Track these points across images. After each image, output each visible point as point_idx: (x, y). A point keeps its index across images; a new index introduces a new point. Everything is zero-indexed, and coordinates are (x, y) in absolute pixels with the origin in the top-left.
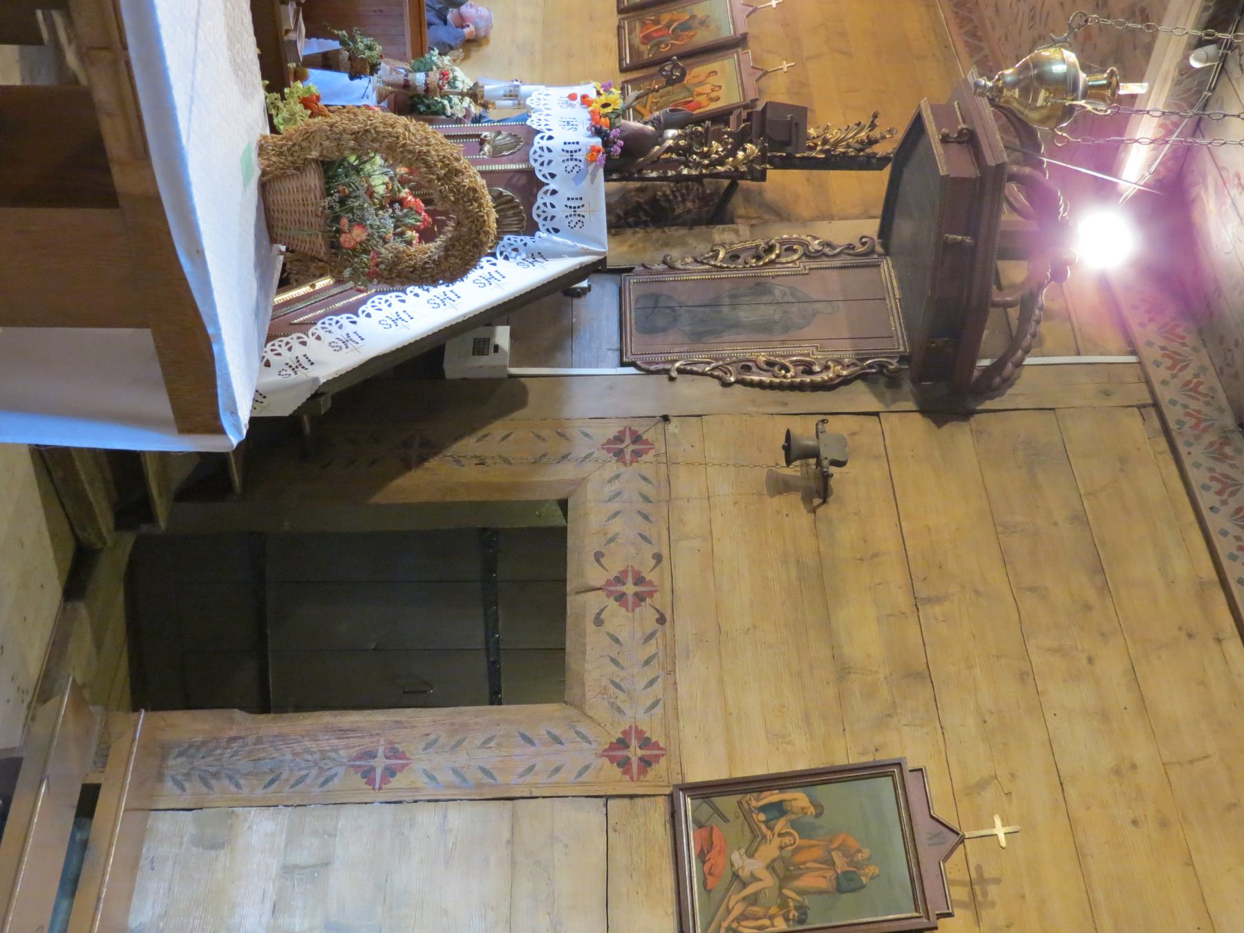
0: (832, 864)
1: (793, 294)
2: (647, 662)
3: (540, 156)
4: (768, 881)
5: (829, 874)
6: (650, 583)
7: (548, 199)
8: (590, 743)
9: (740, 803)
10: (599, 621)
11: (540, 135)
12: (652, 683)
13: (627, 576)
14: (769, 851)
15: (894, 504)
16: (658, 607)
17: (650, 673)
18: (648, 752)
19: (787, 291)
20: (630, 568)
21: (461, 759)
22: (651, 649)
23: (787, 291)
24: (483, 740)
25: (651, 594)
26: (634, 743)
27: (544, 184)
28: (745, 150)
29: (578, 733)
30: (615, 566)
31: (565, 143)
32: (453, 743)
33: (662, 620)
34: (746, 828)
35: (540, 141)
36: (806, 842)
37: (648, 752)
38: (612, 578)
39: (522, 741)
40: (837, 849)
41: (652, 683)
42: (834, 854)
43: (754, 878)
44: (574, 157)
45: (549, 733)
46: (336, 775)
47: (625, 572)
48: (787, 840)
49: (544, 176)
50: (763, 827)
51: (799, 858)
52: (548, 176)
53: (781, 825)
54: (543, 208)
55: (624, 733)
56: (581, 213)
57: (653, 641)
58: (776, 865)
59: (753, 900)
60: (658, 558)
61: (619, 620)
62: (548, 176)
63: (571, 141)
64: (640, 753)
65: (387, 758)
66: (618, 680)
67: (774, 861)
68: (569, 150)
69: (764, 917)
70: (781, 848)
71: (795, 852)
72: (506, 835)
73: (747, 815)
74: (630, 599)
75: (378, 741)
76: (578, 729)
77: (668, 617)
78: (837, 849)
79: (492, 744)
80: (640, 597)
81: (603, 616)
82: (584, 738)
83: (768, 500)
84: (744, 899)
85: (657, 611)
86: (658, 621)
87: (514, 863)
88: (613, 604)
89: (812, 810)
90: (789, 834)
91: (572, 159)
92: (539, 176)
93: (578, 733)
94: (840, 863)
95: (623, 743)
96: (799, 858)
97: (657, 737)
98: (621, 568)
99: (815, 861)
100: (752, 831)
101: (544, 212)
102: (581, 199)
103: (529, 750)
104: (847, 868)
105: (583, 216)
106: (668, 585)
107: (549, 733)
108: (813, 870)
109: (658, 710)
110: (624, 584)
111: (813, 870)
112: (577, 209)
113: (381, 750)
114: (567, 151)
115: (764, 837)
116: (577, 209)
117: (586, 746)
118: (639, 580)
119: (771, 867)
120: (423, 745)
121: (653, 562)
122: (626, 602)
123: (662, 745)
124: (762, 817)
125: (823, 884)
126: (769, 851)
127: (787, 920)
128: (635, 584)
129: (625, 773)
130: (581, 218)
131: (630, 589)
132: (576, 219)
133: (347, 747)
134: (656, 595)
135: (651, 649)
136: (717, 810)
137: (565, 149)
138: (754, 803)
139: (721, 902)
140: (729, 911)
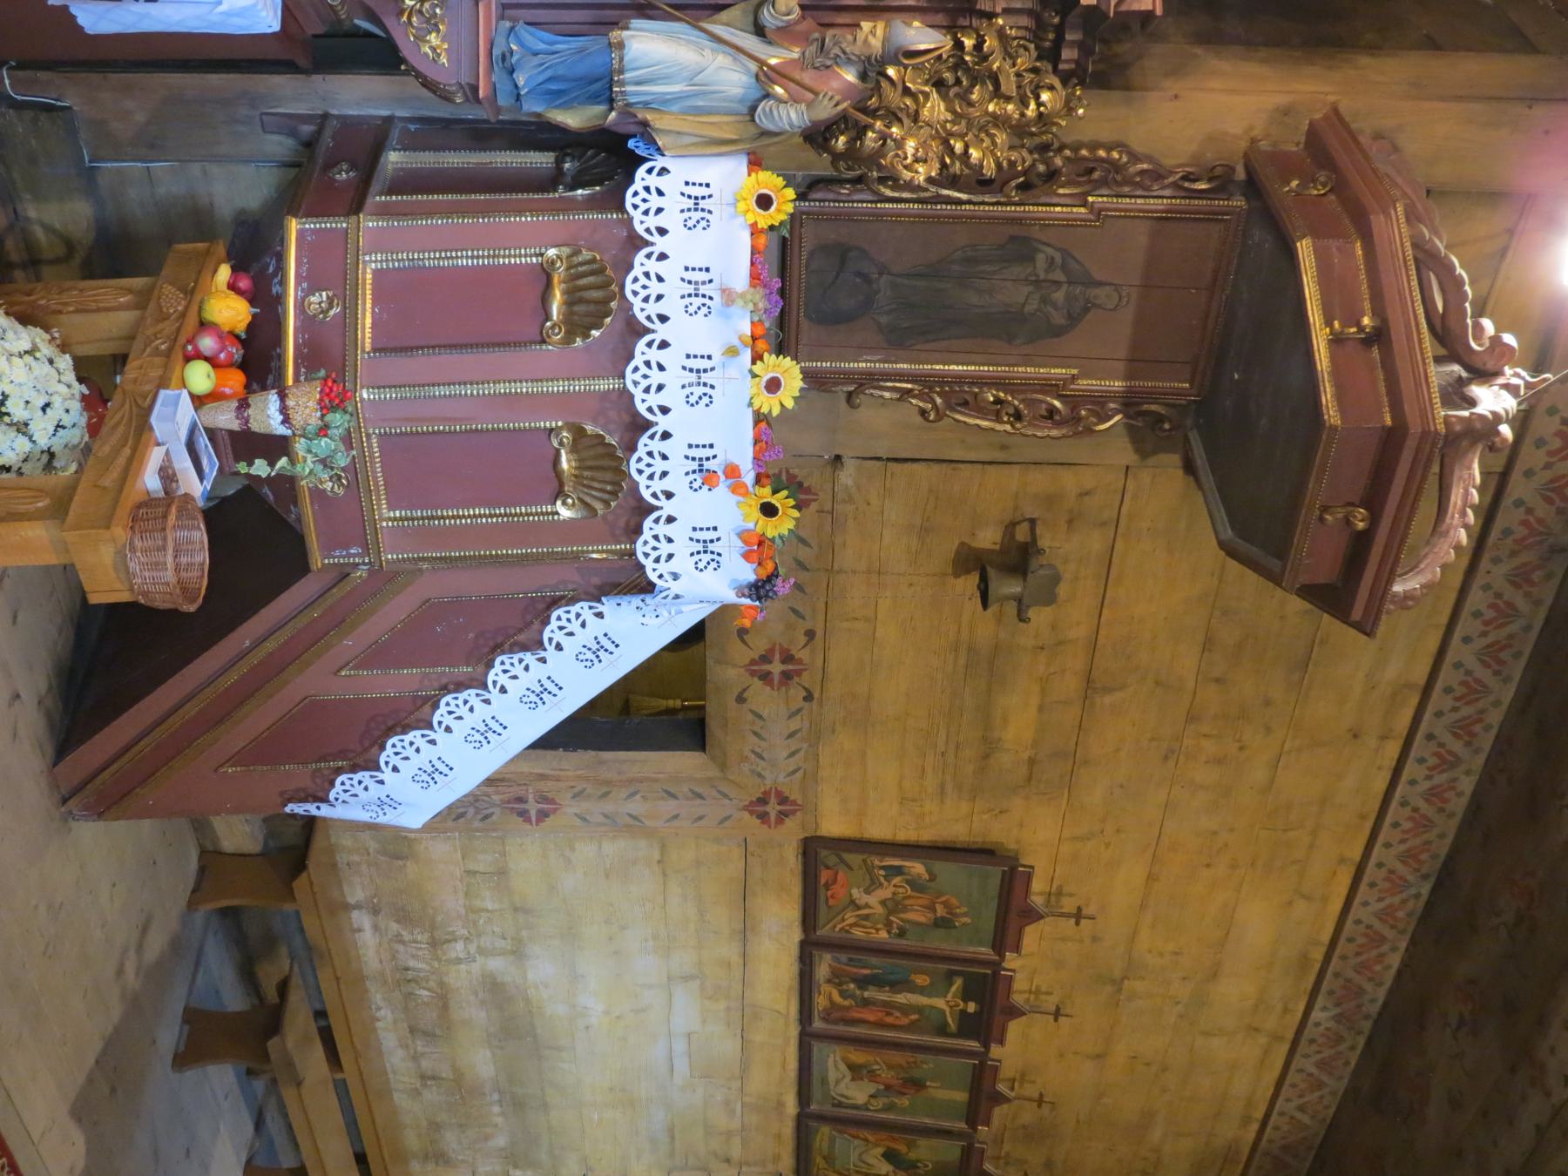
0: (934, 911)
1: (1064, 268)
2: (791, 735)
3: (644, 287)
4: (879, 910)
5: (931, 915)
6: (800, 662)
7: (654, 355)
8: (731, 800)
9: (864, 861)
10: (741, 699)
11: (647, 165)
12: (793, 754)
13: (773, 655)
14: (886, 893)
15: (1104, 582)
16: (807, 686)
17: (794, 744)
18: (790, 667)
19: (1058, 257)
20: (777, 647)
21: (609, 807)
22: (795, 724)
23: (1058, 257)
24: (628, 794)
25: (799, 673)
26: (773, 800)
27: (647, 244)
28: (1050, 41)
29: (719, 792)
30: (760, 645)
31: (690, 446)
32: (600, 794)
33: (809, 697)
34: (868, 876)
35: (646, 349)
36: (914, 894)
37: (790, 667)
38: (757, 657)
39: (666, 796)
40: (941, 903)
41: (793, 754)
42: (937, 905)
43: (867, 906)
44: (693, 201)
45: (691, 790)
46: (492, 814)
47: (771, 651)
48: (901, 890)
49: (650, 410)
50: (882, 879)
51: (907, 902)
52: (656, 410)
53: (897, 880)
54: (644, 370)
55: (765, 793)
56: (707, 207)
57: (799, 717)
58: (888, 903)
59: (866, 918)
60: (810, 634)
61: (764, 698)
62: (656, 410)
63: (697, 267)
64: (779, 808)
65: (538, 803)
66: (759, 750)
67: (886, 900)
68: (702, 539)
69: (871, 928)
70: (894, 894)
71: (905, 898)
72: (656, 855)
73: (870, 870)
74: (776, 678)
75: (527, 790)
76: (720, 789)
77: (816, 695)
78: (941, 903)
79: (638, 797)
80: (787, 676)
81: (745, 695)
82: (725, 796)
83: (951, 580)
84: (858, 916)
85: (806, 689)
86: (805, 699)
87: (665, 875)
88: (757, 683)
89: (927, 877)
90: (903, 887)
91: (696, 210)
92: (646, 495)
93: (719, 792)
94: (941, 911)
95: (763, 801)
96: (907, 902)
97: (795, 795)
98: (767, 647)
99: (921, 906)
100: (872, 880)
101: (645, 376)
102: (708, 185)
103: (672, 803)
104: (945, 915)
105: (710, 212)
106: (819, 663)
107: (691, 790)
108: (917, 911)
109: (799, 775)
110: (770, 662)
111: (917, 911)
112: (700, 201)
113: (531, 797)
114: (694, 459)
115: (881, 885)
116: (704, 462)
117: (727, 801)
118: (788, 658)
119: (883, 903)
120: (570, 795)
121: (803, 640)
122: (772, 680)
123: (799, 802)
124: (882, 872)
125: (922, 919)
126: (886, 893)
127: (889, 932)
128: (783, 662)
129: (763, 823)
130: (708, 390)
131: (776, 668)
132: (699, 390)
133: (497, 793)
134: (805, 674)
135: (795, 724)
136: (843, 861)
137: (691, 455)
138: (877, 863)
139: (839, 914)
140: (843, 920)
